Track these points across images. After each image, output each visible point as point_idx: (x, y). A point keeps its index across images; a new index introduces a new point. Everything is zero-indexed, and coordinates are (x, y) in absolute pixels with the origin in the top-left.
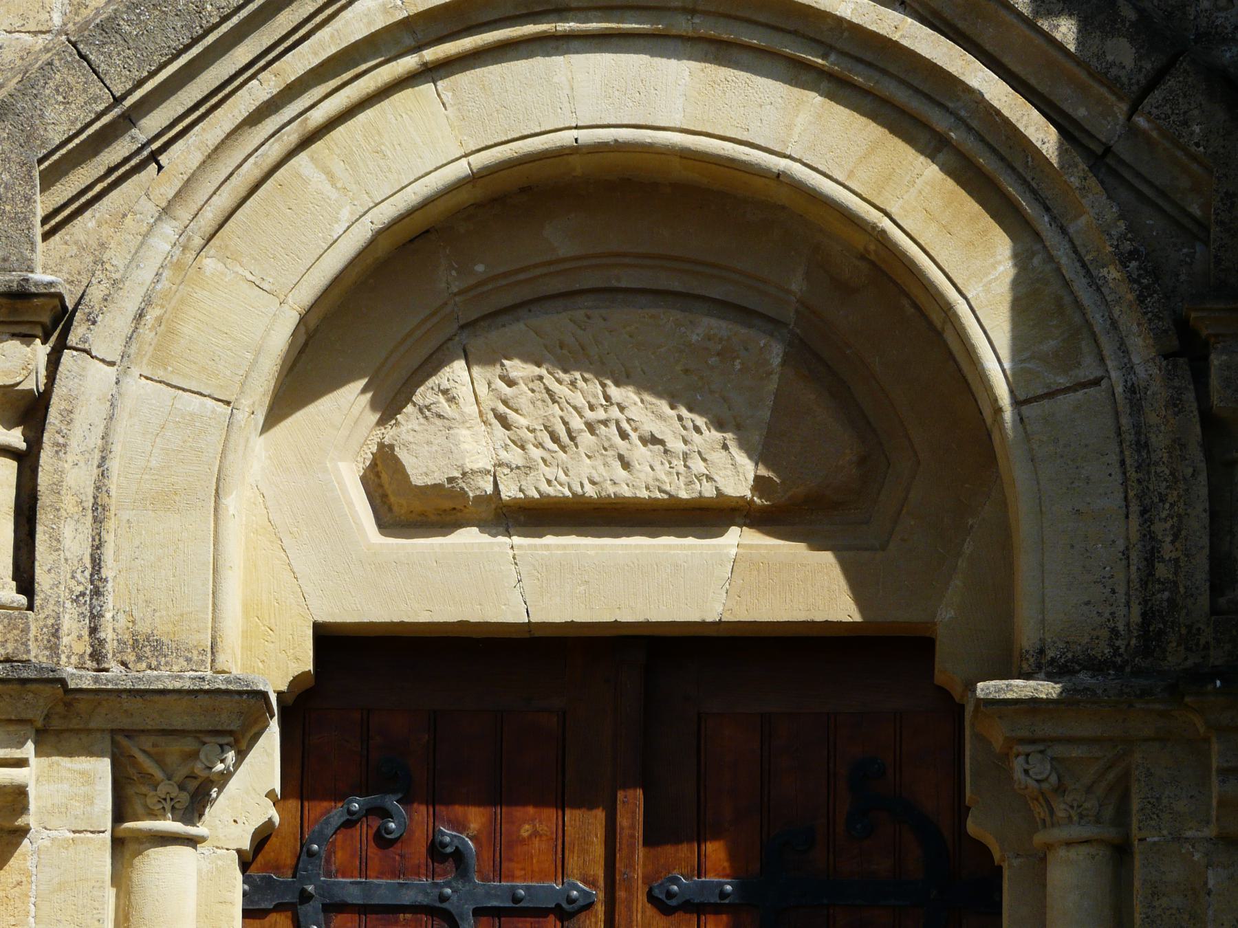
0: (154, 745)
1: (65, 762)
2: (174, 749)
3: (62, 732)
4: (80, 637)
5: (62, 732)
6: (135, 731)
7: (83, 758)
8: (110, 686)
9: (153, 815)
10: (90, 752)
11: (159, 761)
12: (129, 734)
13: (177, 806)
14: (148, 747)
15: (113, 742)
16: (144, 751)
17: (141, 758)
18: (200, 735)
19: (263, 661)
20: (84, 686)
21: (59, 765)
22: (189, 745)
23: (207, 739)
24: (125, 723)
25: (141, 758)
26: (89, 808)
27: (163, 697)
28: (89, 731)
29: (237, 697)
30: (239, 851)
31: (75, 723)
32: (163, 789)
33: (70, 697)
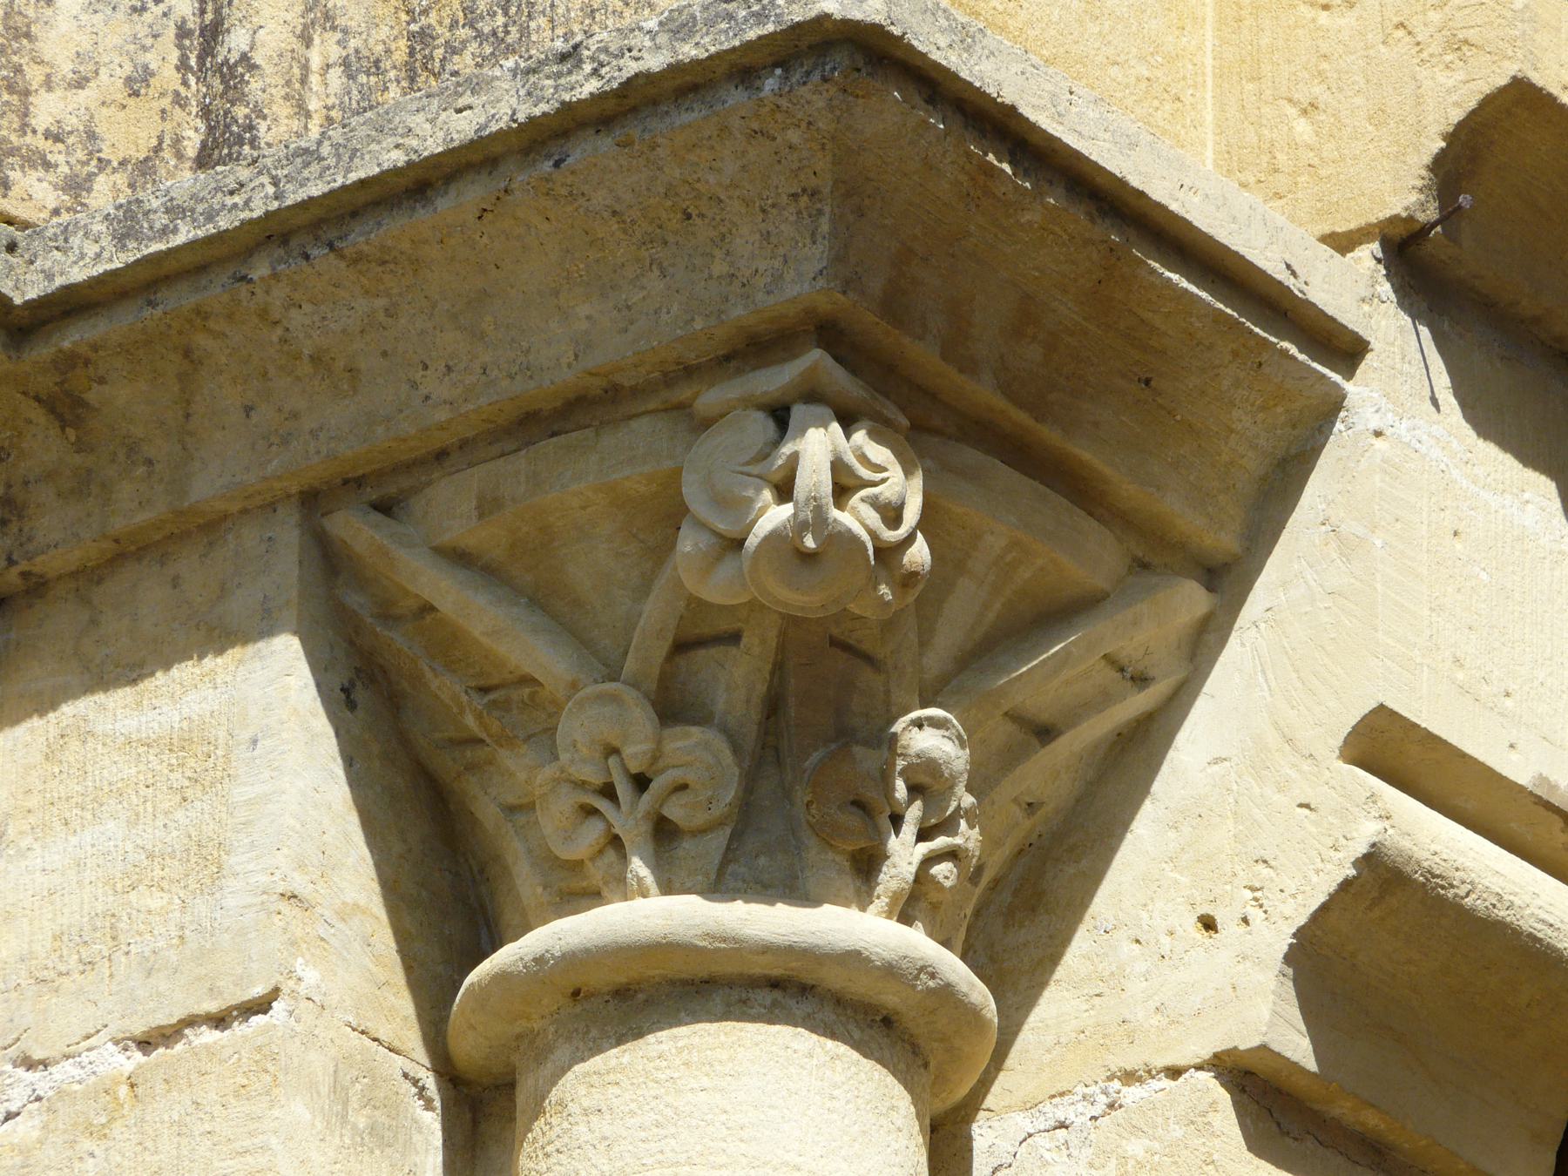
0: (487, 506)
1: (111, 713)
2: (578, 485)
3: (89, 576)
4: (138, 83)
5: (89, 576)
6: (408, 467)
7: (185, 672)
8: (185, 234)
9: (578, 893)
10: (219, 633)
11: (547, 601)
12: (386, 490)
13: (675, 811)
14: (460, 528)
15: (330, 561)
16: (459, 558)
17: (447, 592)
18: (666, 390)
19: (1309, 109)
20: (78, 275)
21: (86, 736)
22: (627, 456)
23: (710, 398)
24: (336, 431)
25: (447, 592)
26: (201, 907)
27: (423, 216)
28: (209, 527)
29: (735, 97)
30: (1253, 1083)
31: (133, 507)
32: (580, 729)
33: (42, 351)
